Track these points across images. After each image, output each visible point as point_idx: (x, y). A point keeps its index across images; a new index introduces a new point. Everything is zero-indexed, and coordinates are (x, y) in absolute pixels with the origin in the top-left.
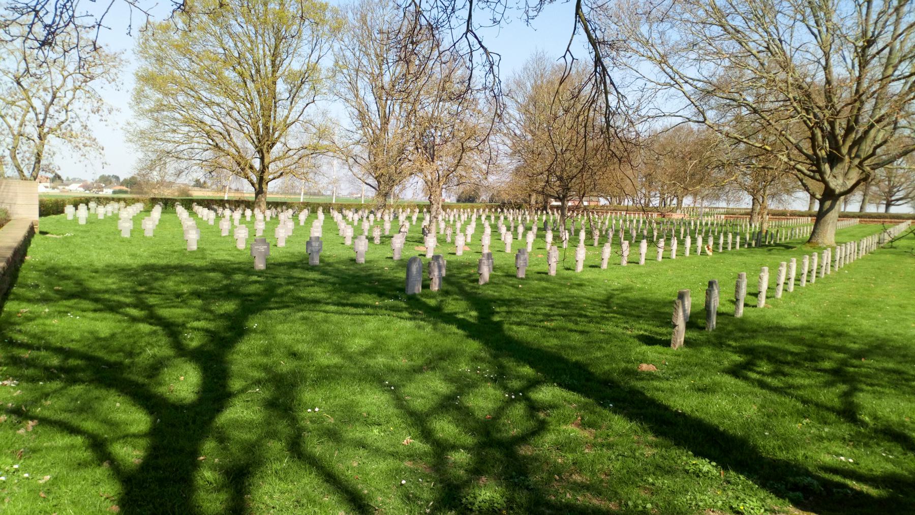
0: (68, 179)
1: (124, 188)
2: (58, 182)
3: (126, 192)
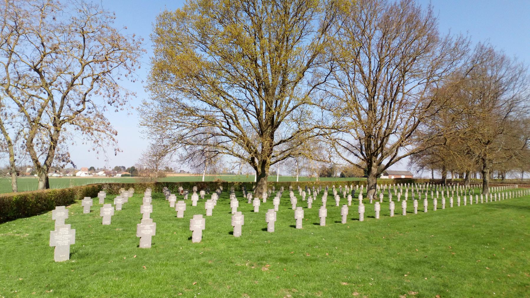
0: (98, 169)
1: (128, 173)
2: (93, 170)
3: (129, 176)
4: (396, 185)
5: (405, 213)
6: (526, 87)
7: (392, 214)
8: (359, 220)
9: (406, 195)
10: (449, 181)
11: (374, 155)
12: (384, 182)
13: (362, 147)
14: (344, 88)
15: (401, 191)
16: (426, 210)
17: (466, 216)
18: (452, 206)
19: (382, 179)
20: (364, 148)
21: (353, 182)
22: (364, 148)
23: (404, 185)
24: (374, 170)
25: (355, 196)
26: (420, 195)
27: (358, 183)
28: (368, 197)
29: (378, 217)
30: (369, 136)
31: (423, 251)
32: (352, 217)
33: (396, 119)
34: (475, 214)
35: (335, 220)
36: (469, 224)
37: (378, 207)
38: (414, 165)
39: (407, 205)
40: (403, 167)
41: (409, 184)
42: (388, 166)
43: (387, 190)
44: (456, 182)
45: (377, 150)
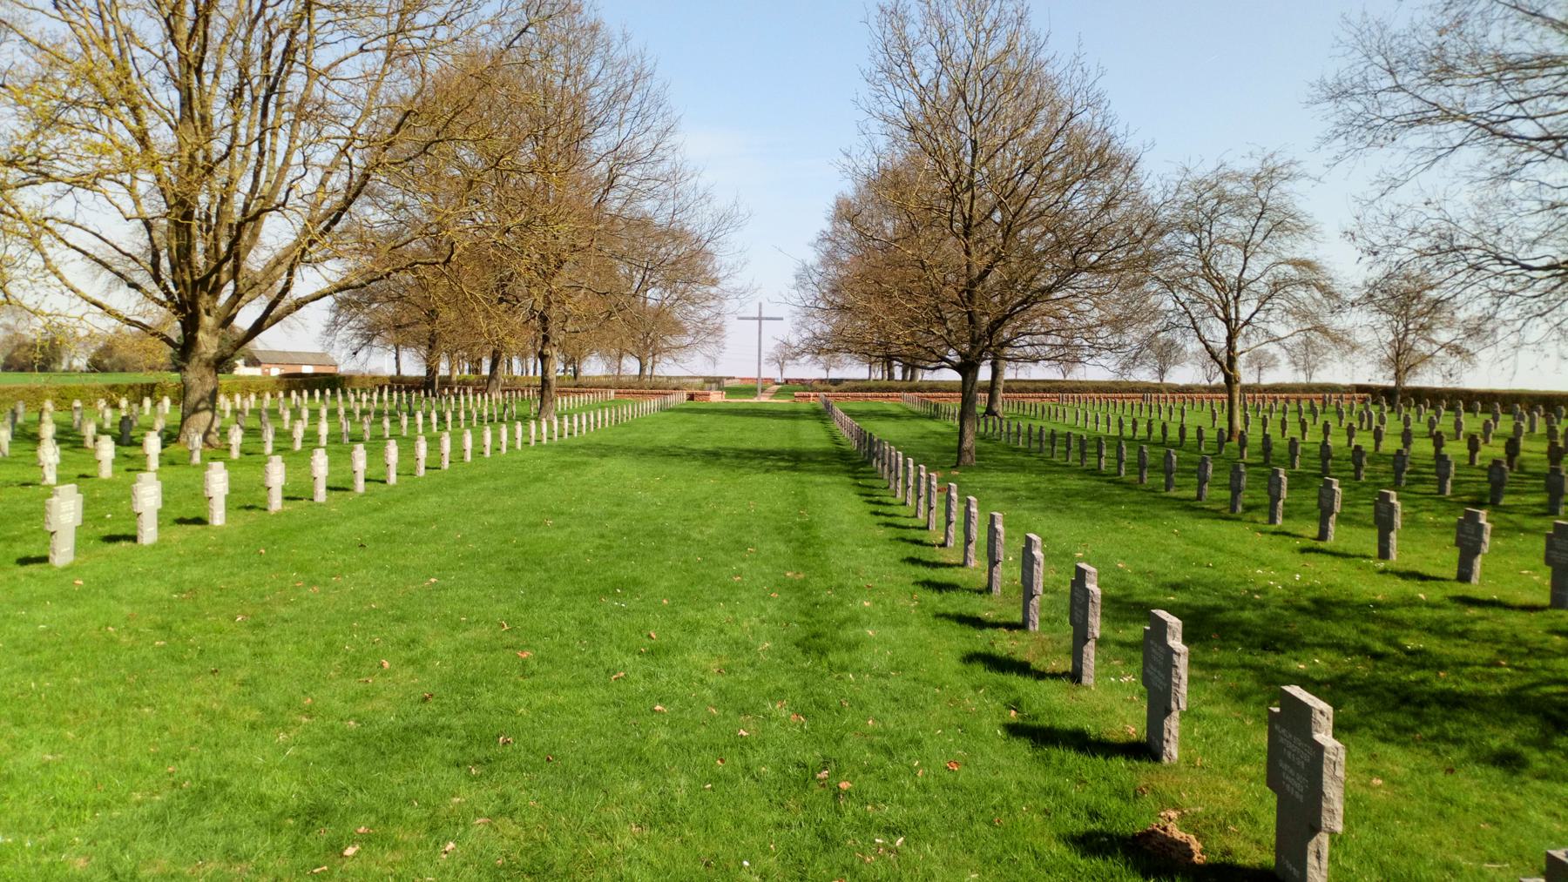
4: (288, 395)
5: (321, 495)
6: (649, 122)
7: (276, 503)
8: (134, 539)
9: (324, 428)
10: (446, 382)
11: (204, 288)
12: (247, 387)
13: (156, 255)
14: (74, 17)
15: (305, 414)
16: (393, 479)
17: (516, 488)
18: (469, 458)
19: (238, 377)
20: (165, 264)
21: (131, 387)
22: (165, 264)
23: (311, 395)
24: (208, 343)
25: (125, 437)
26: (366, 427)
27: (150, 390)
28: (183, 439)
29: (218, 517)
30: (182, 210)
31: (411, 662)
32: (107, 530)
33: (286, 162)
34: (538, 479)
35: (21, 550)
36: (532, 518)
37: (218, 481)
38: (343, 333)
39: (331, 463)
40: (307, 336)
41: (328, 392)
42: (258, 327)
43: (257, 413)
44: (464, 384)
45: (218, 269)
